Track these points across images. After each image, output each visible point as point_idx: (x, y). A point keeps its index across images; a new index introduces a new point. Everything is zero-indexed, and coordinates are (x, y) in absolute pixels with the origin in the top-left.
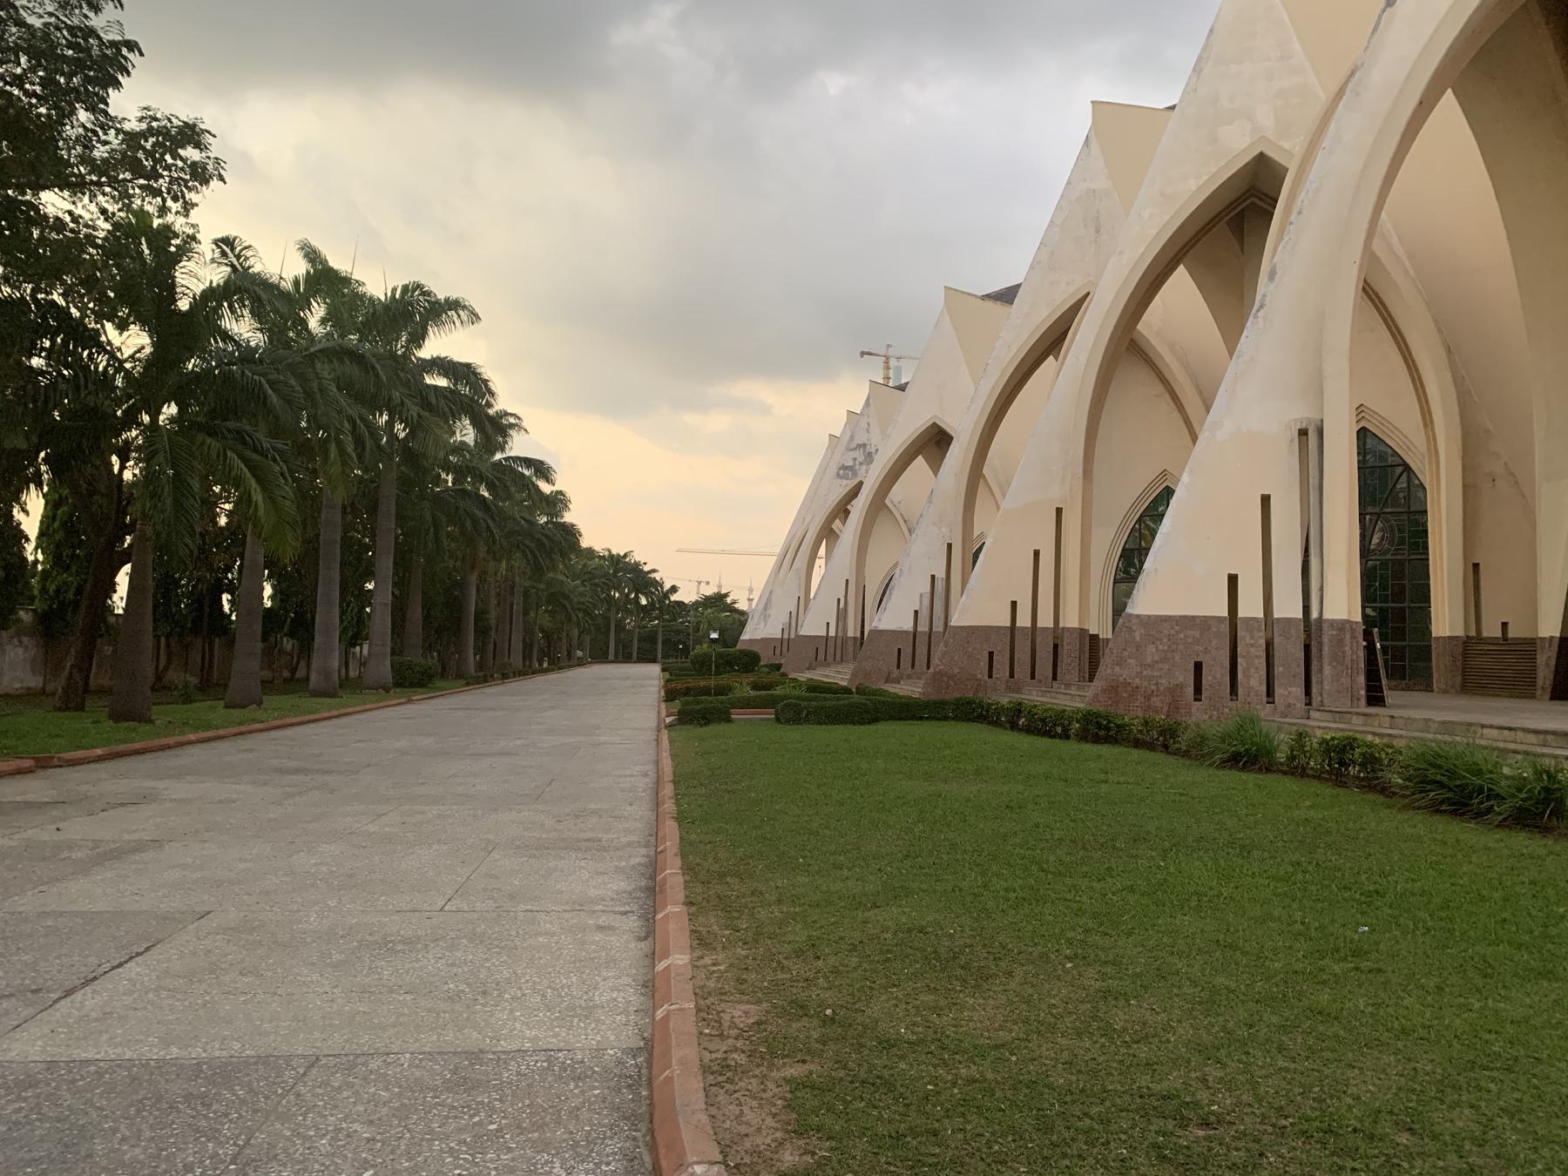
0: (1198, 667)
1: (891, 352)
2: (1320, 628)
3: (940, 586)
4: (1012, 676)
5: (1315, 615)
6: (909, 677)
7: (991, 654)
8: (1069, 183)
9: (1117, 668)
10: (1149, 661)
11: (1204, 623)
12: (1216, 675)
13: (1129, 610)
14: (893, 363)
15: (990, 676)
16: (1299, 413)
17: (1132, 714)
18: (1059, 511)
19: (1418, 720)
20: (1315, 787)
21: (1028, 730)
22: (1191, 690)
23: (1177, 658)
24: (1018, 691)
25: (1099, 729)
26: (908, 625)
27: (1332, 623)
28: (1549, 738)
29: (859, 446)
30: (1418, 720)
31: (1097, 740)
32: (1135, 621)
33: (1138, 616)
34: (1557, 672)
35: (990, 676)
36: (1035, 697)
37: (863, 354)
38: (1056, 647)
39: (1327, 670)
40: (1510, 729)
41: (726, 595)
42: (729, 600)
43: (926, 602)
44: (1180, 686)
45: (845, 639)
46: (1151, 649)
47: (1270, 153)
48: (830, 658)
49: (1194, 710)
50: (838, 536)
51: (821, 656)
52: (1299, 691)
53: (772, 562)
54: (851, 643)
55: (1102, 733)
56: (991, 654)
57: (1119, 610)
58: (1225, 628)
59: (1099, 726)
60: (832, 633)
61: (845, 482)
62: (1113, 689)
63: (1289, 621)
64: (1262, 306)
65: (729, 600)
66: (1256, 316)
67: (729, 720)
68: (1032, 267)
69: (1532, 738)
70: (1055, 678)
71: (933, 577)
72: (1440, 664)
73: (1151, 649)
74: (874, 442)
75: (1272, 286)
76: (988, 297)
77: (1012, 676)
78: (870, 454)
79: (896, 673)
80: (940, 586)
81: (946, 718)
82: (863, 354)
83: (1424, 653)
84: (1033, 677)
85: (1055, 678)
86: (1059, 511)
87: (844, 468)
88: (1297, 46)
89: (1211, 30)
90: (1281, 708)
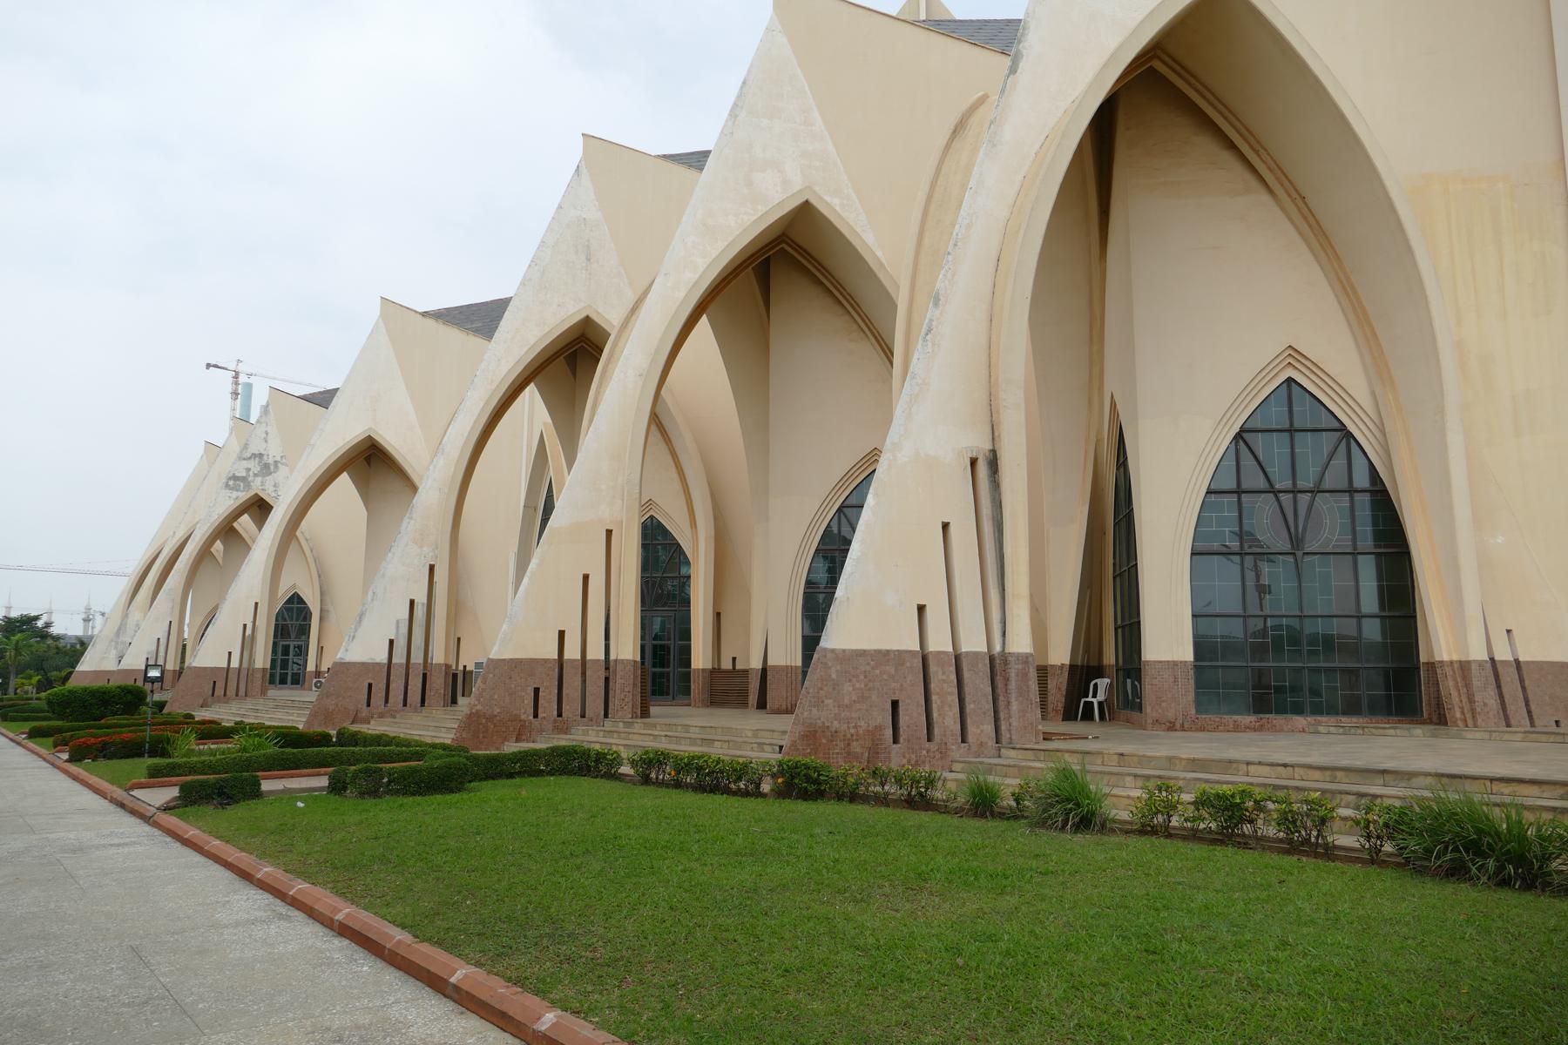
0: (895, 704)
1: (241, 368)
2: (1006, 662)
3: (420, 612)
4: (560, 715)
5: (998, 648)
6: (381, 716)
7: (537, 691)
8: (560, 207)
9: (814, 710)
10: (846, 701)
11: (899, 657)
12: (912, 715)
13: (823, 643)
14: (243, 379)
15: (536, 716)
16: (979, 443)
17: (839, 766)
18: (609, 533)
19: (687, 730)
20: (1388, 873)
21: (700, 788)
22: (889, 732)
23: (874, 697)
24: (566, 731)
25: (801, 783)
26: (382, 657)
27: (1018, 656)
28: (1339, 774)
29: (254, 456)
30: (687, 730)
31: (805, 796)
32: (829, 655)
33: (833, 651)
34: (1067, 697)
35: (536, 716)
36: (589, 737)
37: (209, 366)
38: (425, 676)
39: (1015, 706)
40: (1285, 765)
41: (37, 618)
42: (40, 624)
43: (404, 630)
44: (879, 728)
45: (251, 671)
46: (847, 687)
47: (814, 202)
48: (231, 691)
49: (893, 754)
50: (249, 548)
51: (219, 691)
52: (989, 728)
53: (123, 585)
54: (259, 675)
55: (812, 788)
56: (537, 691)
57: (810, 644)
58: (918, 663)
59: (808, 779)
60: (235, 664)
61: (235, 494)
62: (811, 736)
63: (976, 654)
64: (929, 331)
65: (40, 624)
66: (925, 340)
67: (255, 793)
68: (523, 284)
69: (1317, 775)
70: (606, 715)
71: (412, 602)
72: (696, 686)
73: (847, 687)
74: (271, 453)
75: (937, 312)
76: (425, 314)
77: (560, 715)
78: (267, 466)
79: (365, 712)
80: (420, 612)
81: (540, 773)
82: (209, 366)
83: (686, 677)
84: (583, 716)
85: (606, 715)
86: (609, 533)
87: (235, 478)
88: (816, 114)
89: (744, 83)
90: (974, 748)
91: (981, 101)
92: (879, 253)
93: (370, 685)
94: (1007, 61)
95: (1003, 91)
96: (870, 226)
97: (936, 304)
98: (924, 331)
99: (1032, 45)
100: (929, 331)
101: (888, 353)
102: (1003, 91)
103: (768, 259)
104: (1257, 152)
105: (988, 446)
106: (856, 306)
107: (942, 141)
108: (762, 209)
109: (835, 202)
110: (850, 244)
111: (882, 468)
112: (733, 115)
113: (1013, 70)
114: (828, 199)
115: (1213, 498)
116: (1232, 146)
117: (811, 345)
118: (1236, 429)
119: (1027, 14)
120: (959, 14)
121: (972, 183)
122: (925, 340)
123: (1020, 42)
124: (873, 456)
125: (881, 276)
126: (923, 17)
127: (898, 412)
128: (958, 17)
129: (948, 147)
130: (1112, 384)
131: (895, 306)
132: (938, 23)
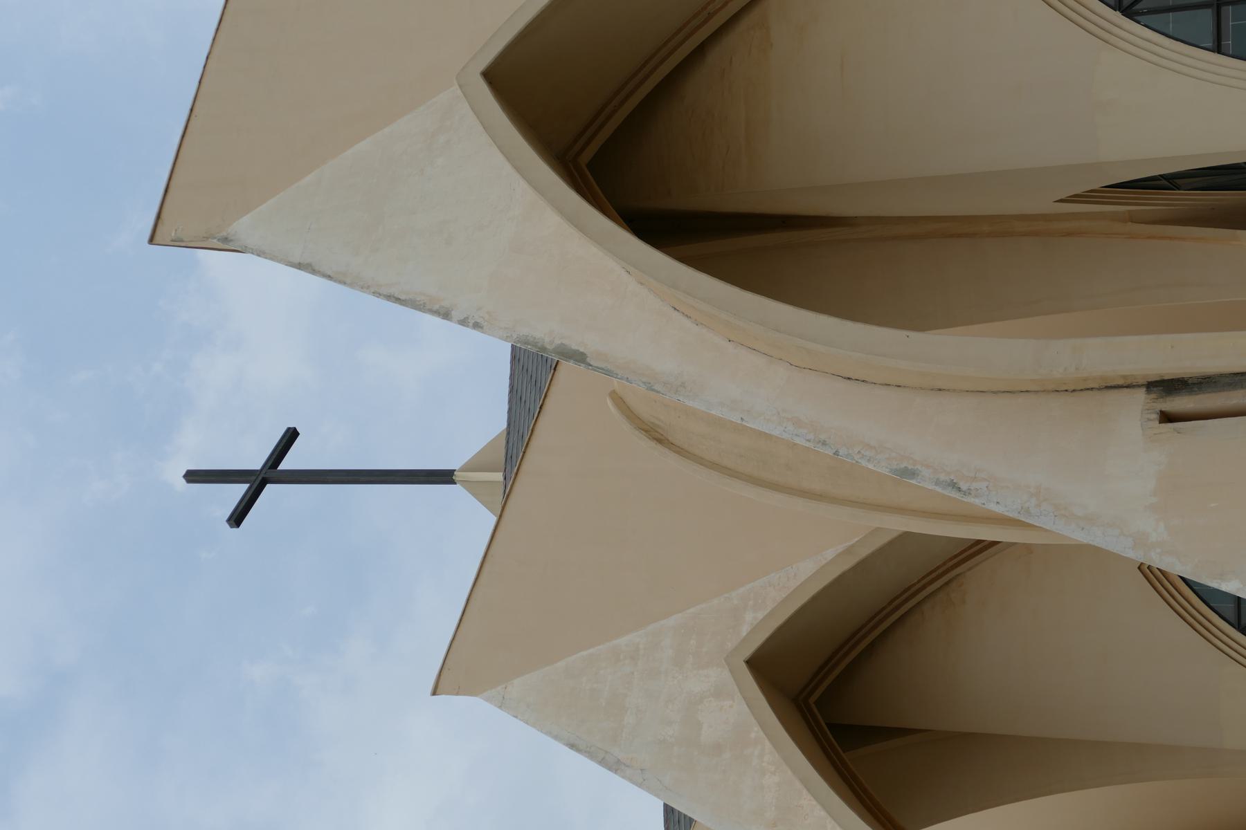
47: (748, 651)
64: (953, 485)
66: (967, 493)
88: (623, 641)
89: (572, 746)
91: (620, 402)
92: (830, 554)
93: (193, 476)
94: (566, 367)
95: (608, 373)
96: (789, 568)
97: (913, 474)
98: (954, 494)
99: (547, 331)
100: (953, 485)
101: (979, 548)
102: (608, 373)
103: (830, 726)
104: (711, 16)
105: (1141, 394)
106: (908, 593)
107: (671, 461)
108: (756, 732)
109: (751, 618)
110: (780, 630)
111: (1177, 567)
112: (615, 766)
113: (579, 358)
114: (745, 630)
115: (1228, 43)
116: (701, 50)
117: (985, 663)
118: (1116, 16)
119: (506, 339)
120: (498, 422)
121: (735, 418)
122: (967, 493)
123: (544, 349)
124: (1154, 576)
125: (864, 552)
126: (499, 476)
127: (1080, 537)
128: (505, 426)
129: (680, 451)
130: (1042, 202)
131: (906, 536)
132: (509, 458)
